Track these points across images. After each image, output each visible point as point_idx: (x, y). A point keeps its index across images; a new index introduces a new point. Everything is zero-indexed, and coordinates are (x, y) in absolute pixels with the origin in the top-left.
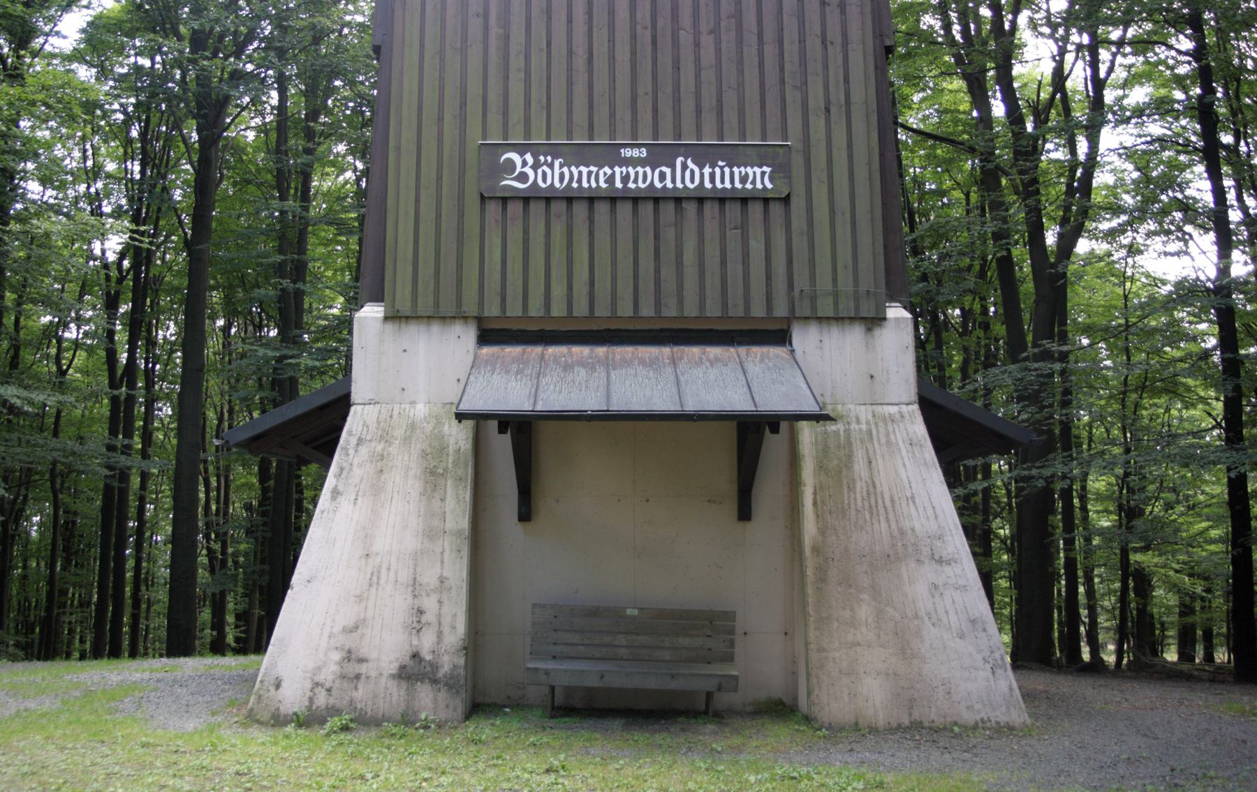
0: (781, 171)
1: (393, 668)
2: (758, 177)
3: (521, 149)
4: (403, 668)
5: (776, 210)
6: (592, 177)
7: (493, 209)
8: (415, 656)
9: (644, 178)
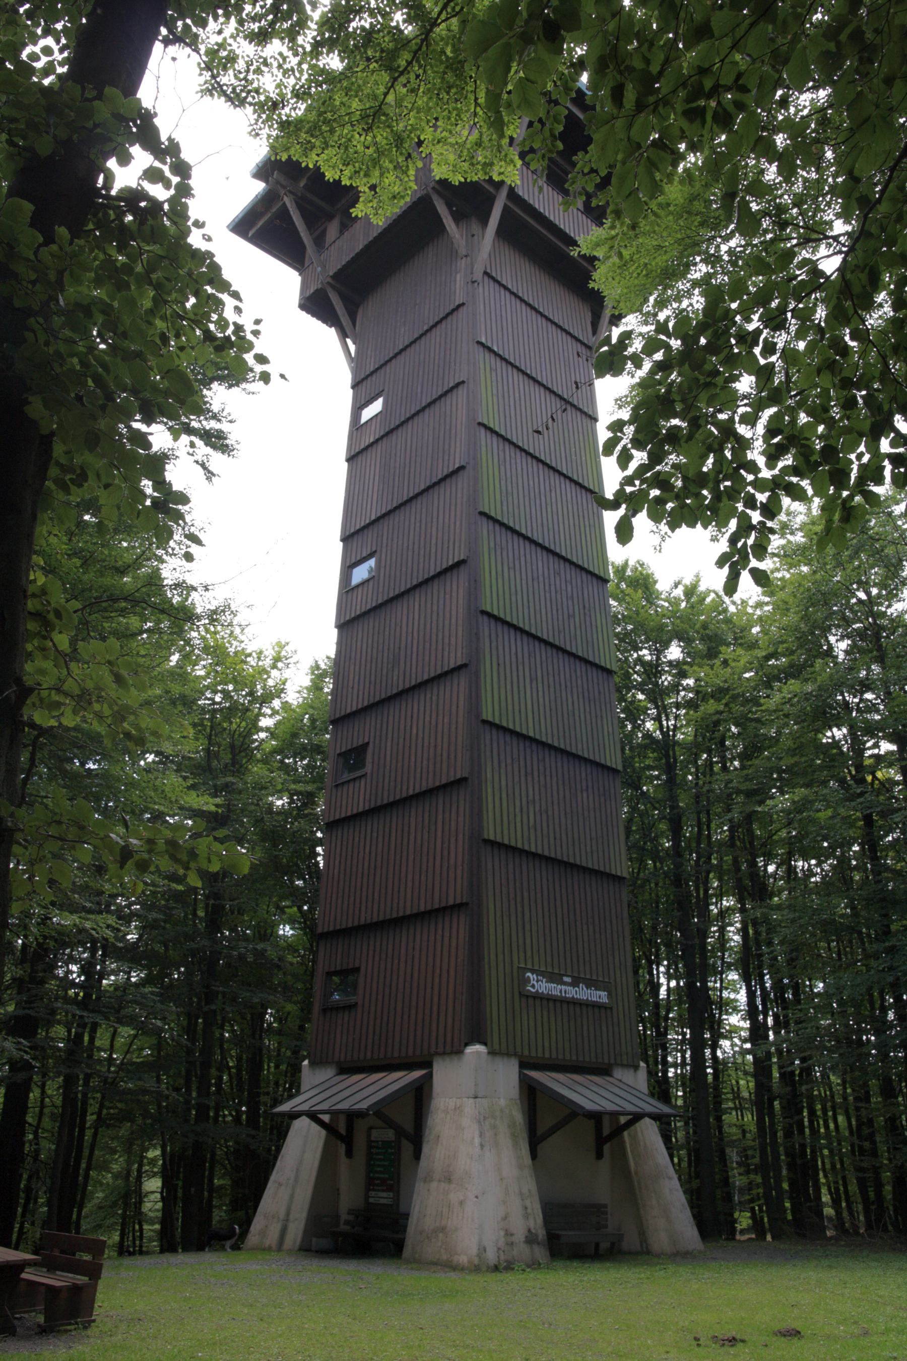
0: (610, 996)
1: (523, 1239)
2: (601, 996)
3: (533, 971)
4: (727, 1239)
5: (609, 1011)
6: (555, 989)
7: (524, 1000)
8: (529, 1231)
9: (571, 992)
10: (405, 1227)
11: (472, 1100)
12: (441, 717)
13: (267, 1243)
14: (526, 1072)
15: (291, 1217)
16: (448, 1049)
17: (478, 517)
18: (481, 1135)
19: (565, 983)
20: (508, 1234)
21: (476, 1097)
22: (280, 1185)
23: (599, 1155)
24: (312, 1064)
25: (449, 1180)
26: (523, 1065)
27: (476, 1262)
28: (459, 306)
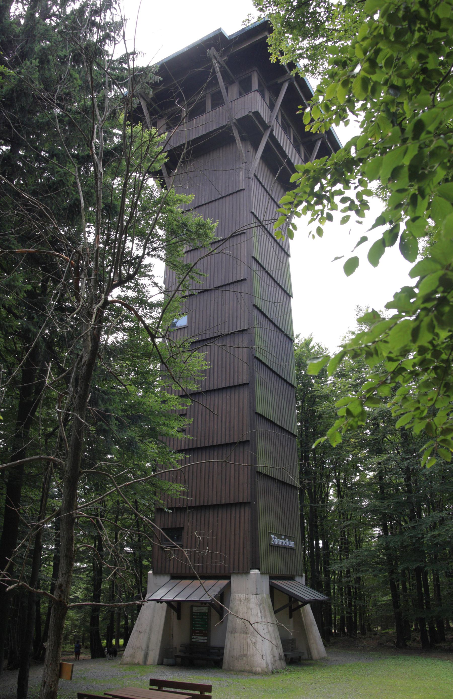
3: (273, 534)
10: (223, 654)
11: (254, 596)
12: (233, 408)
13: (136, 661)
14: (274, 581)
15: (150, 648)
16: (241, 571)
17: (252, 307)
18: (261, 612)
19: (282, 539)
20: (274, 657)
21: (257, 594)
22: (140, 632)
23: (291, 617)
24: (154, 573)
25: (246, 632)
26: (271, 578)
27: (266, 670)
28: (241, 190)
